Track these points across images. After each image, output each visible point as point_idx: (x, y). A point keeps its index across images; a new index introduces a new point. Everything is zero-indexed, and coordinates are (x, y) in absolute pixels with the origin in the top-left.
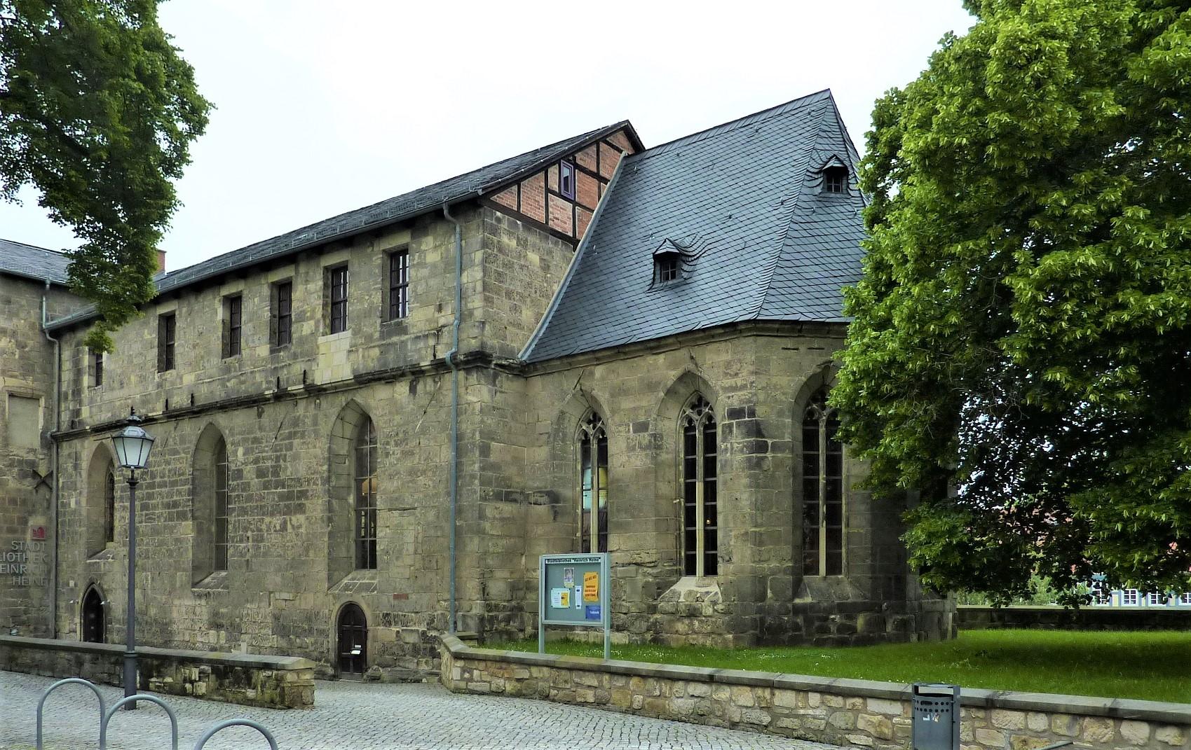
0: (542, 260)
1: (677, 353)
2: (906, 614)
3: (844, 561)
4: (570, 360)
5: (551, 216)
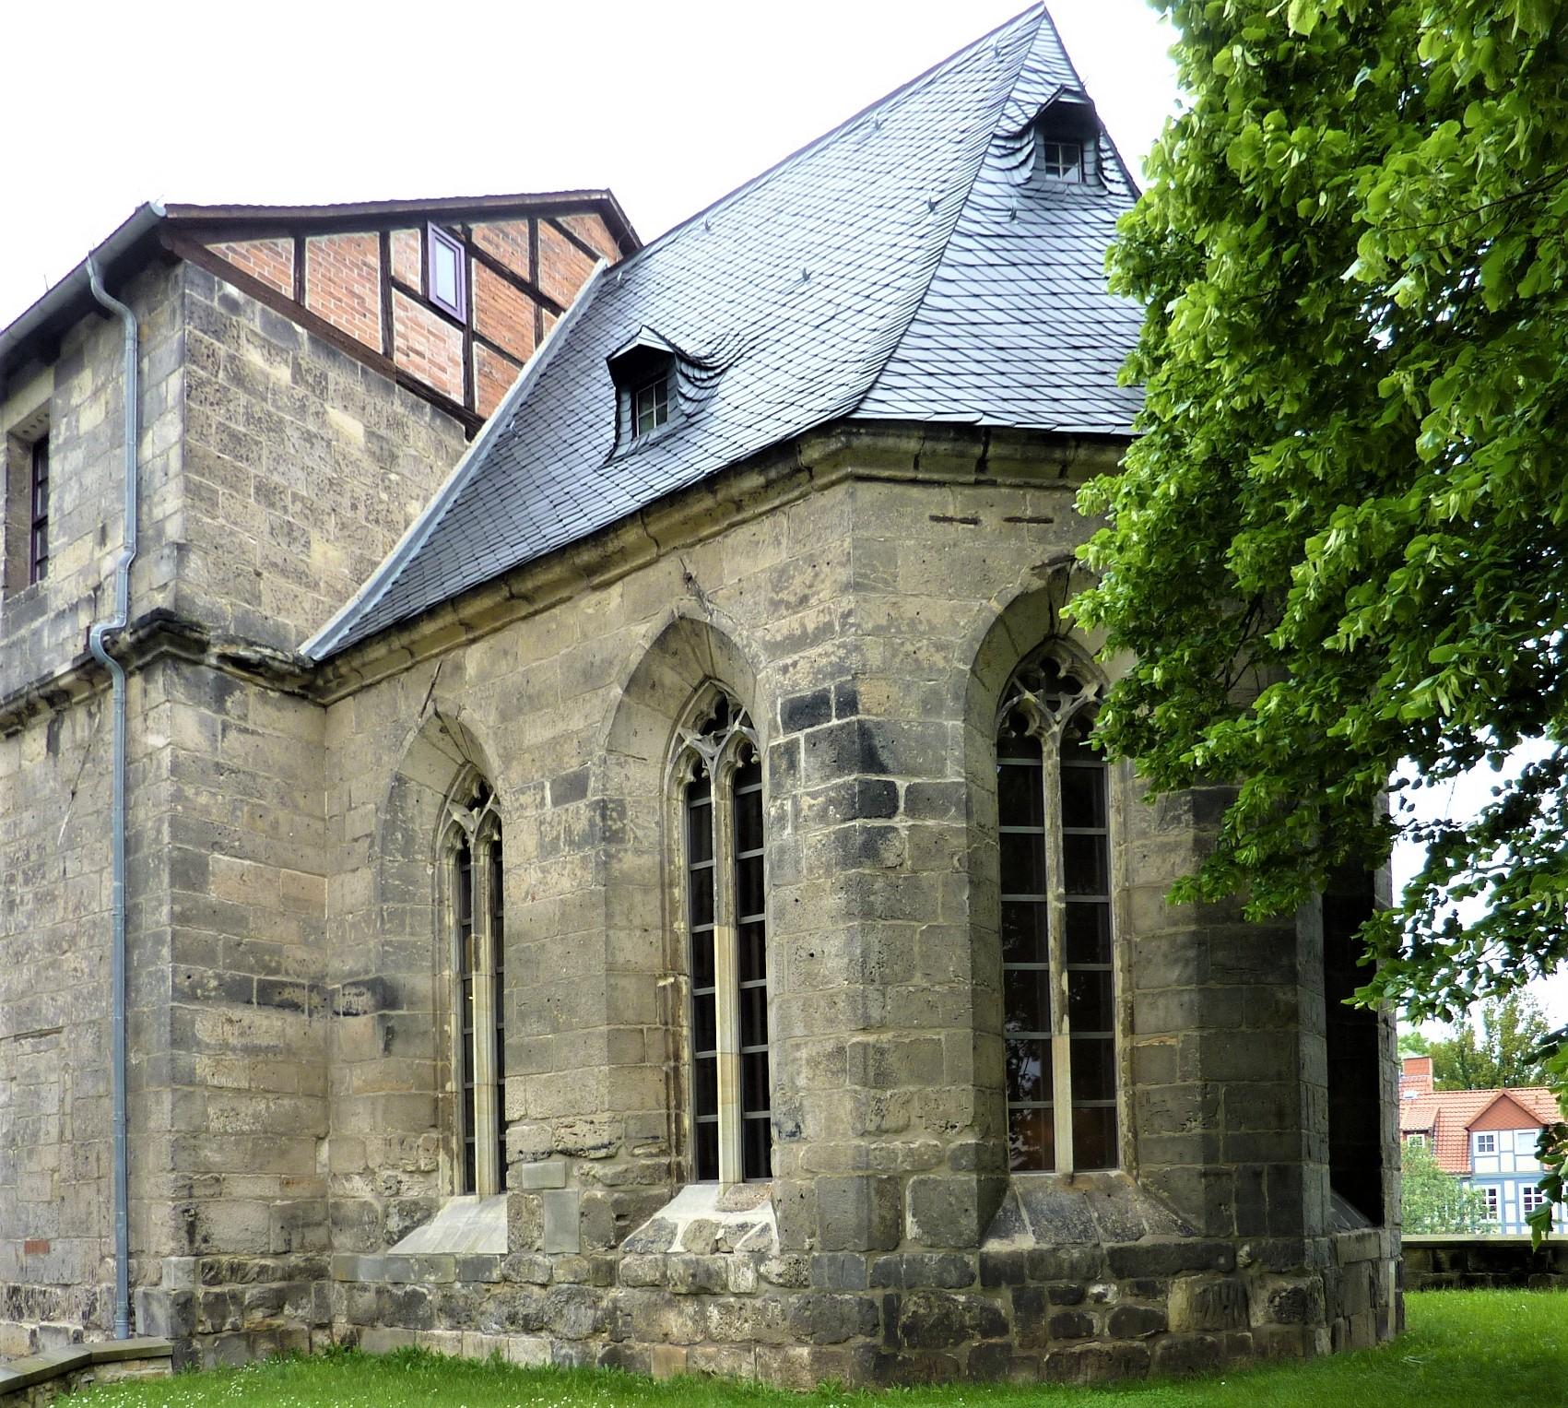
0: (371, 435)
1: (652, 574)
2: (1302, 1273)
3: (1123, 1130)
4: (405, 639)
5: (398, 342)
